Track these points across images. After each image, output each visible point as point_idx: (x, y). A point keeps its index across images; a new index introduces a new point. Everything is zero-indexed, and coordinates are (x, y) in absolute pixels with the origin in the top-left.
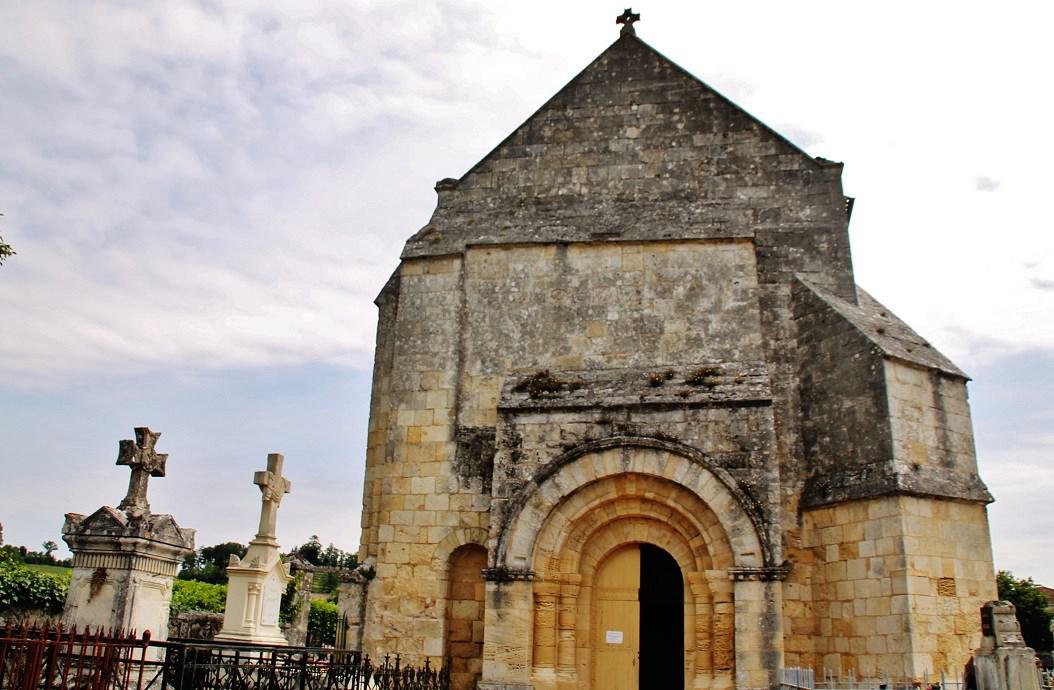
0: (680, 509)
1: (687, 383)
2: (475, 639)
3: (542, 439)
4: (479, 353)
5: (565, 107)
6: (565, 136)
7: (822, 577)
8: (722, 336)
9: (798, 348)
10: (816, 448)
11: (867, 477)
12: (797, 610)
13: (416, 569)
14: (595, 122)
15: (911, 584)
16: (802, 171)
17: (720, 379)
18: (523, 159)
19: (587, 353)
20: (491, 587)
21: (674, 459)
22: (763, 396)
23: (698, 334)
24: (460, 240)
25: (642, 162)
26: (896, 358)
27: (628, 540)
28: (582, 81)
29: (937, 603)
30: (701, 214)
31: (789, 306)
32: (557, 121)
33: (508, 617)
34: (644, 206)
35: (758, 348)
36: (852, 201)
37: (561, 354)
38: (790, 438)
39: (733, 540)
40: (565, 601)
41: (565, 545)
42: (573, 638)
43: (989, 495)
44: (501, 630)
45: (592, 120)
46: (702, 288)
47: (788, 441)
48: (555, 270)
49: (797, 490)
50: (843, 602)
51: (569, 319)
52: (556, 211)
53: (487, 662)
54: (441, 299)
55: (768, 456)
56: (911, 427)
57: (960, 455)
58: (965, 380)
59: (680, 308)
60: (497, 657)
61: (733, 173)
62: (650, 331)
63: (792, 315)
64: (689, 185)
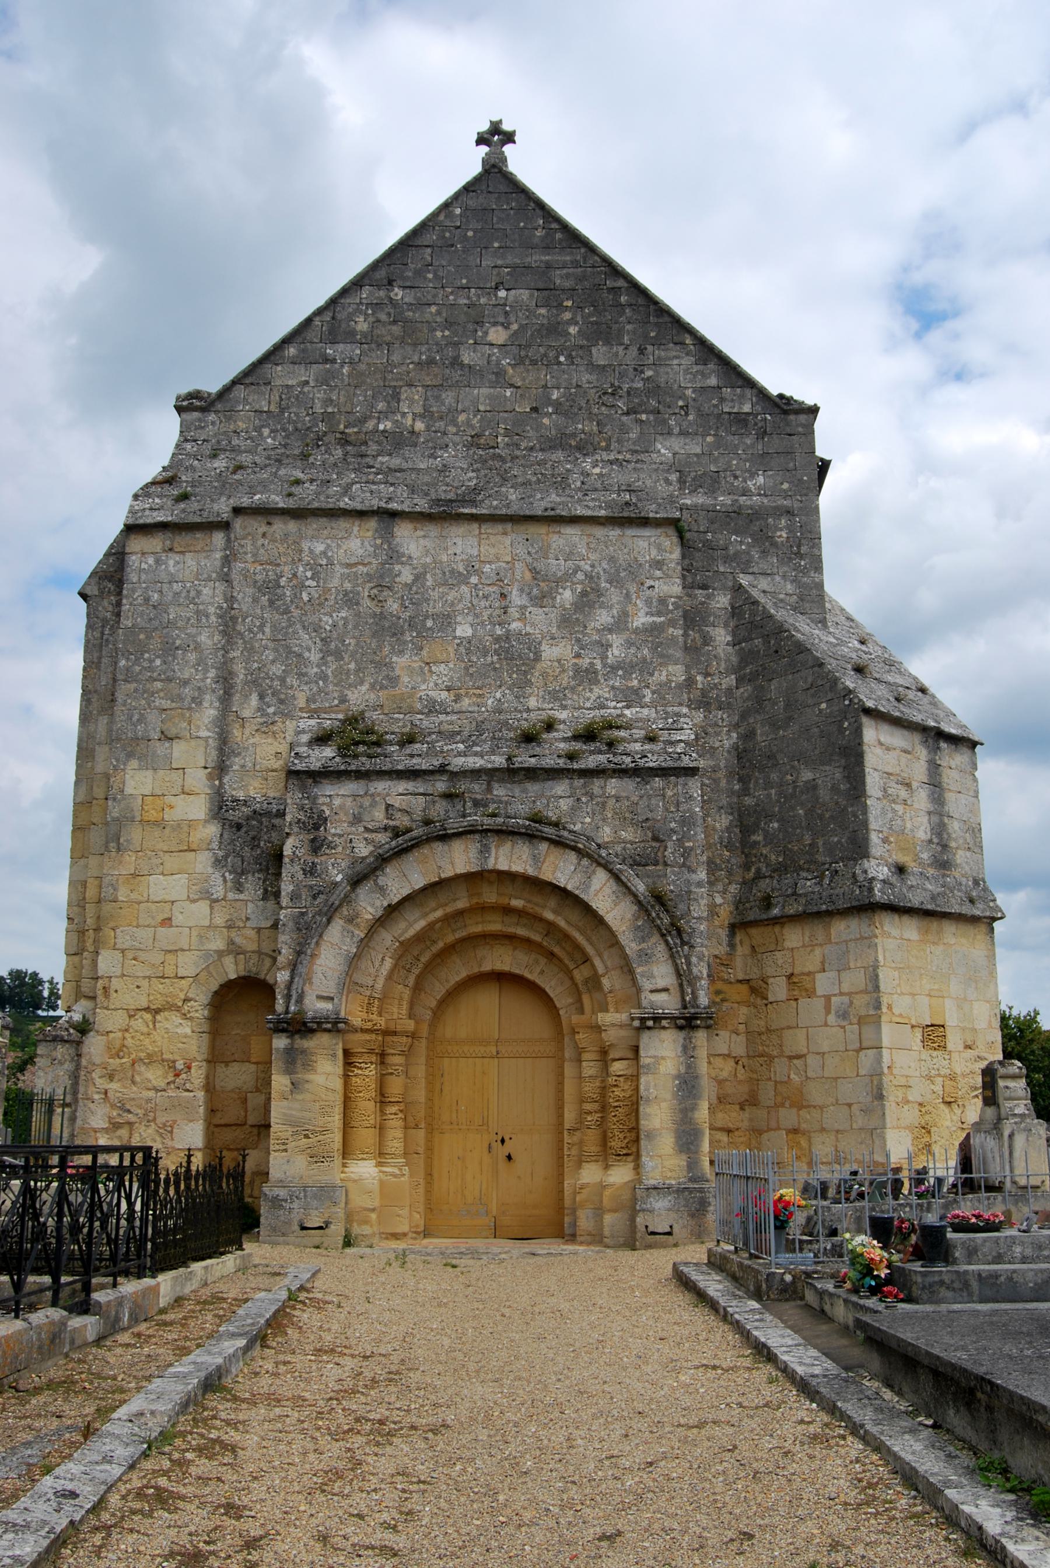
0: (562, 924)
2: (252, 1120)
3: (357, 819)
5: (390, 283)
7: (762, 1023)
8: (626, 668)
10: (758, 837)
12: (726, 1068)
14: (439, 313)
15: (888, 1034)
17: (622, 733)
18: (321, 366)
19: (424, 687)
20: (280, 1042)
22: (686, 762)
23: (592, 664)
24: (223, 499)
25: (512, 386)
27: (482, 969)
28: (419, 242)
29: (920, 1060)
30: (600, 475)
31: (726, 626)
33: (306, 1086)
34: (514, 458)
35: (679, 686)
38: (722, 822)
39: (639, 970)
40: (391, 1060)
41: (389, 977)
42: (401, 1115)
43: (998, 909)
44: (297, 1105)
45: (433, 309)
46: (599, 592)
48: (376, 556)
49: (729, 896)
50: (791, 1058)
51: (396, 633)
52: (375, 457)
54: (193, 594)
55: (692, 849)
56: (894, 811)
57: (960, 852)
58: (973, 744)
59: (565, 621)
60: (291, 1145)
61: (651, 412)
62: (519, 655)
63: (729, 638)
64: (584, 426)
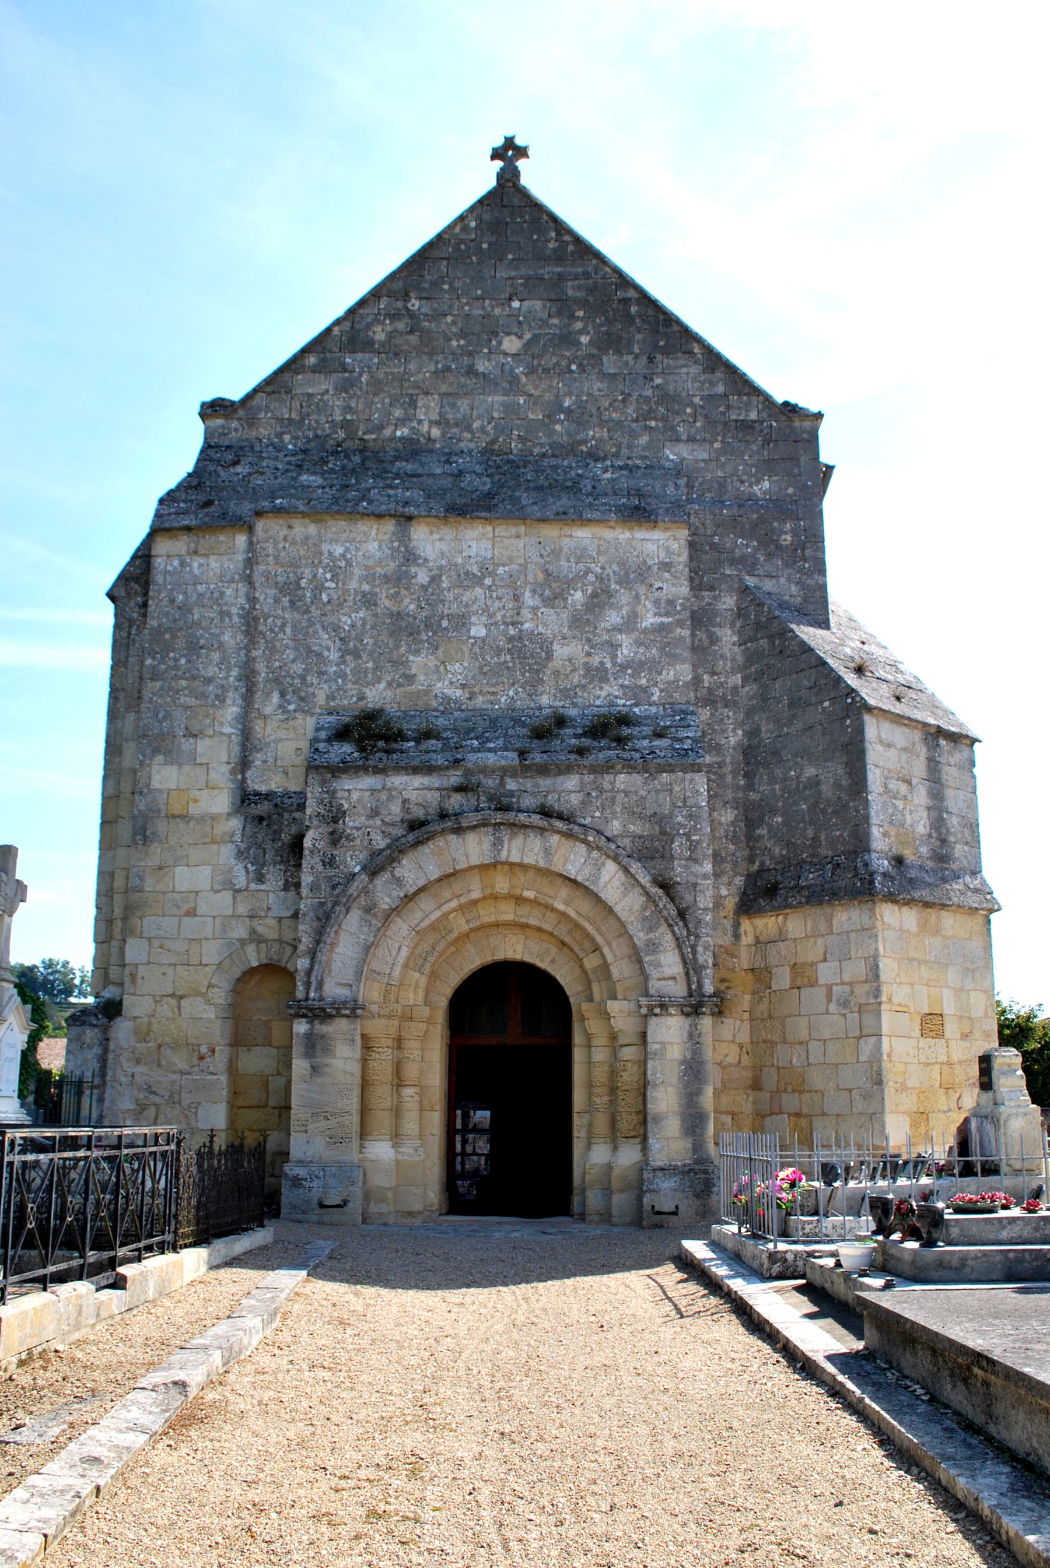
1: (584, 734)
3: (374, 813)
4: (276, 680)
6: (407, 343)
8: (636, 666)
9: (743, 687)
10: (762, 831)
11: (833, 874)
13: (182, 1002)
14: (454, 323)
16: (762, 422)
18: (340, 375)
19: (439, 685)
20: (301, 1027)
21: (567, 844)
23: (602, 663)
25: (525, 394)
26: (881, 710)
32: (395, 317)
33: (326, 1069)
35: (686, 684)
36: (830, 469)
37: (399, 685)
38: (727, 816)
39: (646, 959)
45: (449, 319)
46: (609, 594)
47: (723, 819)
48: (393, 558)
51: (413, 633)
52: (392, 463)
53: (297, 1134)
54: (216, 595)
55: (698, 842)
56: (895, 807)
58: (974, 741)
60: (311, 1126)
63: (735, 639)
